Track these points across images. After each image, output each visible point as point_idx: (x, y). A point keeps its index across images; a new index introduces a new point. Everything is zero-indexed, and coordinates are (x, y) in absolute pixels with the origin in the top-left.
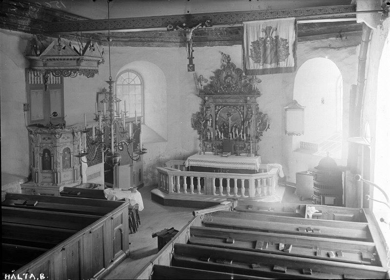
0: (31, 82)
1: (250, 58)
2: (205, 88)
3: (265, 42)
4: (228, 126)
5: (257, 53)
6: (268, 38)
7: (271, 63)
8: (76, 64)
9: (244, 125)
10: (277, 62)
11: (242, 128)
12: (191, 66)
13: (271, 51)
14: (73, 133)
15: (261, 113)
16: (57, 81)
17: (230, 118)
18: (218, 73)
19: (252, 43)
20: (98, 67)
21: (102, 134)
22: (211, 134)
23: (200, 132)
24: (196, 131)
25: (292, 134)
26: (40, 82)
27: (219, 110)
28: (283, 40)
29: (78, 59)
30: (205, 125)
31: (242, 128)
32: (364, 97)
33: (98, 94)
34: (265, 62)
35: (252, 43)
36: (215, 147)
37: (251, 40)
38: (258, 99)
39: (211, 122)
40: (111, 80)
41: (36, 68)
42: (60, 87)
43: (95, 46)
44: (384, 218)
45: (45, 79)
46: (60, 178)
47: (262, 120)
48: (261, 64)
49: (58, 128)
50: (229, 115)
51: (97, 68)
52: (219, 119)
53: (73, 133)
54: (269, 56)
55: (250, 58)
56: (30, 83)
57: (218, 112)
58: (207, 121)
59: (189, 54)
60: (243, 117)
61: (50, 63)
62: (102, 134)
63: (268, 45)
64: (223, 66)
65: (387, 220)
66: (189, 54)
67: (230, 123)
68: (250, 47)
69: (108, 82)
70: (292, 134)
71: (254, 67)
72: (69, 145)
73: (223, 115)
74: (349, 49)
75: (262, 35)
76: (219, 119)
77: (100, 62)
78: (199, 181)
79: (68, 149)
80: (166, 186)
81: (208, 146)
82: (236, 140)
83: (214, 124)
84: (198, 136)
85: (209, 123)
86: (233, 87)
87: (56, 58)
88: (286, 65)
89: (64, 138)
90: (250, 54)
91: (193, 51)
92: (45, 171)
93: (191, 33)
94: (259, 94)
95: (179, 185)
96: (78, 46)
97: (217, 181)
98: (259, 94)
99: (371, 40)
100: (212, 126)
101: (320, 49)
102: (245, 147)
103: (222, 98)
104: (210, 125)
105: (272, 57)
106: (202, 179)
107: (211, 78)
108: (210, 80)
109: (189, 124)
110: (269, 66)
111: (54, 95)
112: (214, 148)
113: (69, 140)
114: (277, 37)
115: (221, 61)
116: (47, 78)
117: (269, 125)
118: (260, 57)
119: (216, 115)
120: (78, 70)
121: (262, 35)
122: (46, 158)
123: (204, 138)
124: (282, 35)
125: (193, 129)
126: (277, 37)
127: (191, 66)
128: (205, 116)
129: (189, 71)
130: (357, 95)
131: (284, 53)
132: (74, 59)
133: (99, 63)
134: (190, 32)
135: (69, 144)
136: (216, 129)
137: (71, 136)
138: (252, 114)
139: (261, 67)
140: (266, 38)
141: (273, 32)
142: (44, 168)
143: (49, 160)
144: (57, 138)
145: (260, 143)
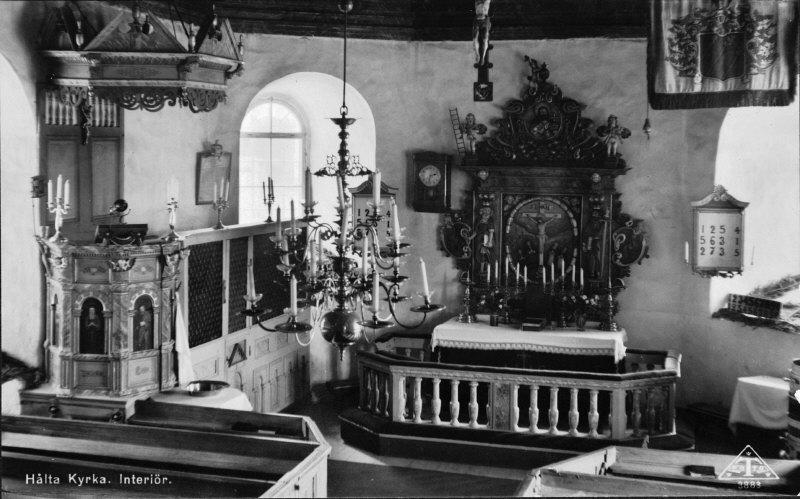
0: (51, 119)
3: (710, 22)
4: (537, 248)
5: (687, 49)
7: (725, 79)
8: (175, 75)
11: (575, 254)
12: (483, 86)
14: (162, 260)
16: (109, 120)
17: (542, 229)
20: (225, 84)
21: (284, 253)
23: (460, 264)
27: (514, 207)
31: (575, 254)
33: (199, 156)
38: (620, 179)
40: (344, 114)
41: (66, 82)
43: (223, 29)
44: (301, 488)
46: (127, 376)
48: (698, 78)
49: (127, 242)
51: (223, 87)
53: (162, 260)
56: (47, 122)
57: (511, 210)
59: (481, 57)
62: (284, 253)
64: (527, 90)
65: (297, 494)
66: (481, 57)
67: (542, 241)
68: (667, 34)
69: (337, 121)
71: (678, 87)
72: (148, 289)
77: (231, 70)
78: (474, 391)
79: (145, 301)
88: (767, 83)
91: (490, 47)
92: (88, 356)
95: (419, 403)
96: (181, 34)
97: (525, 392)
103: (522, 175)
106: (483, 388)
107: (494, 121)
110: (719, 86)
111: (102, 159)
113: (150, 275)
115: (521, 80)
116: (87, 112)
117: (647, 249)
120: (180, 91)
122: (90, 321)
125: (440, 253)
127: (483, 86)
128: (476, 221)
129: (476, 99)
133: (228, 74)
142: (137, 348)
144: (121, 270)
145: (622, 296)
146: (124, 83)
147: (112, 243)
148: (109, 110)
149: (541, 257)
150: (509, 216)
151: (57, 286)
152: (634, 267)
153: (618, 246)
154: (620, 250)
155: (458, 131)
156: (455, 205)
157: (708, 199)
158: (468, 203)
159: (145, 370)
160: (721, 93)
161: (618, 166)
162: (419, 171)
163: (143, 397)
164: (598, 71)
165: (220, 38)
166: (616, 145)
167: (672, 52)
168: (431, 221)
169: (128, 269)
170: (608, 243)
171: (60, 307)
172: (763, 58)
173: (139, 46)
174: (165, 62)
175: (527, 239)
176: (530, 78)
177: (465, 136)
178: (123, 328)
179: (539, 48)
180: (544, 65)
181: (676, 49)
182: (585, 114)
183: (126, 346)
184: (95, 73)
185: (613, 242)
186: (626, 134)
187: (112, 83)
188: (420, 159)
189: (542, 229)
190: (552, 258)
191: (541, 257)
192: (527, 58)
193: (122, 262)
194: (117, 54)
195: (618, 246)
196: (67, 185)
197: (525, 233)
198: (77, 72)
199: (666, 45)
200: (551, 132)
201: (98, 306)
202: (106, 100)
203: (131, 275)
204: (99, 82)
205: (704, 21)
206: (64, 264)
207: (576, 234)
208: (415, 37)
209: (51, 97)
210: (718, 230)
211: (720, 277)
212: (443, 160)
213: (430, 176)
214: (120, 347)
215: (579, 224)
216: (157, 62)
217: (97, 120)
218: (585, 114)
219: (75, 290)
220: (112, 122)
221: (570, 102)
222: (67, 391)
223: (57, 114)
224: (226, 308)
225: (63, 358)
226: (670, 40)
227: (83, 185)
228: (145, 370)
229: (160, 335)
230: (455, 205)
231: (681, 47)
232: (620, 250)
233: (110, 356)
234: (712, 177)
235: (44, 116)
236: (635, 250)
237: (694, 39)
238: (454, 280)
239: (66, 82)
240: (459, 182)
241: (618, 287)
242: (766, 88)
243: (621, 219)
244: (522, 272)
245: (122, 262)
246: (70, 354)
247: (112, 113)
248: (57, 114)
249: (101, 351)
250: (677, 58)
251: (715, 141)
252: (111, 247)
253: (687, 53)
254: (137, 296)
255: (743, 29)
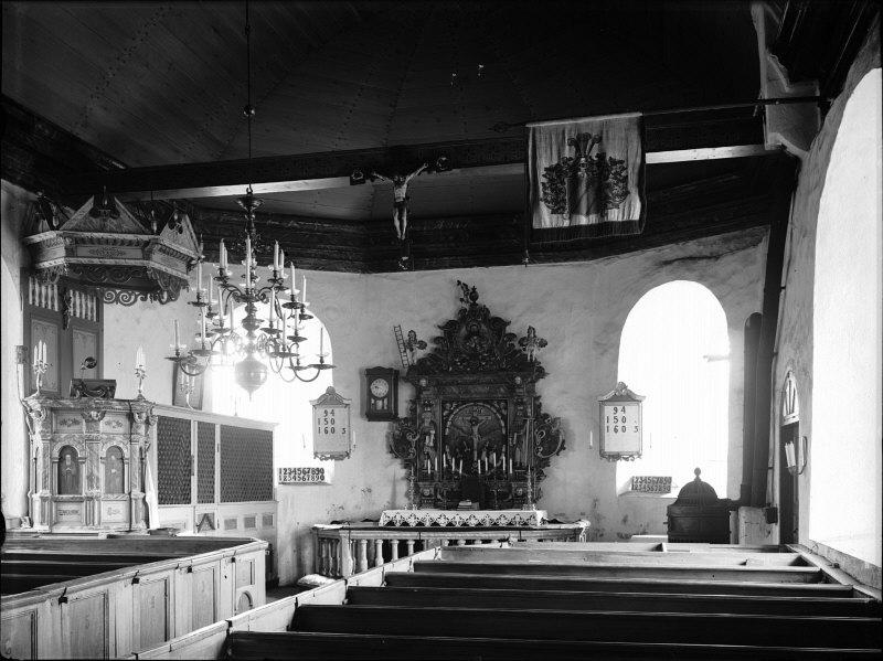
0: (34, 300)
1: (542, 204)
2: (421, 361)
3: (575, 167)
4: (472, 447)
5: (557, 191)
6: (583, 159)
7: (588, 214)
8: (140, 256)
9: (506, 443)
10: (601, 205)
11: (504, 450)
13: (588, 188)
15: (546, 416)
18: (450, 328)
19: (546, 169)
22: (433, 465)
24: (399, 461)
25: (617, 457)
26: (53, 306)
27: (451, 412)
28: (614, 162)
29: (147, 243)
30: (420, 445)
31: (504, 450)
32: (774, 379)
34: (575, 210)
35: (546, 169)
36: (442, 495)
37: (543, 163)
39: (432, 437)
41: (46, 264)
42: (95, 327)
45: (64, 302)
47: (548, 432)
50: (474, 422)
52: (450, 433)
54: (585, 197)
55: (542, 204)
57: (448, 415)
58: (425, 434)
60: (506, 426)
61: (83, 250)
63: (582, 173)
67: (476, 440)
68: (542, 180)
70: (617, 457)
72: (118, 441)
73: (459, 422)
74: (741, 253)
75: (568, 152)
76: (452, 432)
80: (336, 566)
81: (427, 492)
82: (491, 477)
83: (440, 445)
84: (403, 472)
85: (430, 441)
86: (484, 359)
87: (96, 235)
88: (621, 215)
89: (108, 423)
90: (541, 193)
93: (405, 186)
94: (541, 373)
98: (541, 373)
99: (784, 288)
100: (435, 447)
101: (676, 263)
102: (510, 492)
104: (432, 444)
105: (591, 200)
107: (436, 340)
108: (431, 346)
109: (386, 457)
112: (439, 497)
113: (121, 430)
114: (601, 156)
115: (455, 304)
117: (564, 441)
118: (564, 200)
119: (444, 423)
121: (568, 152)
123: (418, 476)
124: (613, 153)
125: (390, 456)
126: (601, 156)
130: (768, 331)
131: (617, 190)
132: (138, 243)
134: (402, 183)
135: (119, 438)
136: (444, 451)
137: (124, 421)
138: (525, 415)
139: (566, 223)
140: (578, 158)
141: (592, 146)
143: (73, 471)
145: (543, 484)
146: (96, 261)
147: (85, 396)
148: (89, 306)
149: (476, 453)
150: (447, 420)
151: (37, 439)
152: (553, 459)
153: (539, 440)
154: (541, 444)
155: (401, 346)
156: (403, 412)
157: (612, 393)
158: (413, 410)
159: (117, 512)
160: (586, 226)
161: (536, 371)
162: (370, 384)
163: (113, 532)
164: (516, 292)
165: (181, 231)
166: (536, 352)
167: (545, 193)
168: (382, 428)
169: (99, 420)
170: (530, 439)
171: (40, 461)
172: (617, 195)
173: (108, 229)
174: (130, 243)
175: (463, 439)
176: (462, 300)
177: (408, 351)
178: (95, 472)
179: (472, 275)
180: (474, 289)
181: (549, 191)
182: (509, 330)
183: (98, 488)
184: (70, 252)
185: (535, 437)
186: (543, 344)
187: (85, 261)
188: (372, 374)
189: (476, 429)
190: (484, 453)
191: (476, 453)
192: (459, 282)
193: (94, 413)
194: (88, 234)
195: (539, 440)
196: (45, 346)
197: (462, 434)
198: (55, 254)
199: (541, 187)
200: (481, 345)
201: (74, 453)
202: (86, 294)
203: (102, 426)
204: (73, 260)
205: (571, 168)
206: (43, 416)
207: (504, 432)
208: (364, 271)
209: (34, 281)
210: (619, 429)
211: (623, 461)
212: (392, 376)
213: (381, 388)
214: (92, 487)
215: (506, 424)
216: (123, 242)
217: (78, 311)
218: (509, 330)
219: (52, 440)
220: (92, 317)
221: (498, 320)
222: (46, 528)
223: (46, 299)
224: (194, 480)
225: (43, 499)
226: (543, 184)
227: (63, 354)
228: (117, 512)
229: (131, 484)
230: (403, 412)
231: (552, 191)
232: (541, 444)
233: (84, 495)
234: (616, 377)
235: (27, 297)
236: (552, 441)
237: (563, 183)
238: (402, 479)
239: (46, 264)
240: (405, 393)
241: (540, 476)
242: (620, 220)
243: (542, 419)
244: (457, 465)
245: (94, 413)
246: (49, 495)
247: (92, 308)
248: (46, 299)
249: (77, 493)
250: (549, 199)
251: (616, 346)
252: (84, 399)
253: (557, 194)
254: (109, 445)
255: (601, 173)
